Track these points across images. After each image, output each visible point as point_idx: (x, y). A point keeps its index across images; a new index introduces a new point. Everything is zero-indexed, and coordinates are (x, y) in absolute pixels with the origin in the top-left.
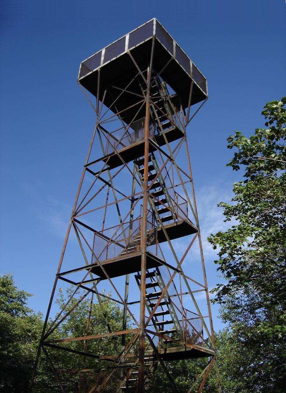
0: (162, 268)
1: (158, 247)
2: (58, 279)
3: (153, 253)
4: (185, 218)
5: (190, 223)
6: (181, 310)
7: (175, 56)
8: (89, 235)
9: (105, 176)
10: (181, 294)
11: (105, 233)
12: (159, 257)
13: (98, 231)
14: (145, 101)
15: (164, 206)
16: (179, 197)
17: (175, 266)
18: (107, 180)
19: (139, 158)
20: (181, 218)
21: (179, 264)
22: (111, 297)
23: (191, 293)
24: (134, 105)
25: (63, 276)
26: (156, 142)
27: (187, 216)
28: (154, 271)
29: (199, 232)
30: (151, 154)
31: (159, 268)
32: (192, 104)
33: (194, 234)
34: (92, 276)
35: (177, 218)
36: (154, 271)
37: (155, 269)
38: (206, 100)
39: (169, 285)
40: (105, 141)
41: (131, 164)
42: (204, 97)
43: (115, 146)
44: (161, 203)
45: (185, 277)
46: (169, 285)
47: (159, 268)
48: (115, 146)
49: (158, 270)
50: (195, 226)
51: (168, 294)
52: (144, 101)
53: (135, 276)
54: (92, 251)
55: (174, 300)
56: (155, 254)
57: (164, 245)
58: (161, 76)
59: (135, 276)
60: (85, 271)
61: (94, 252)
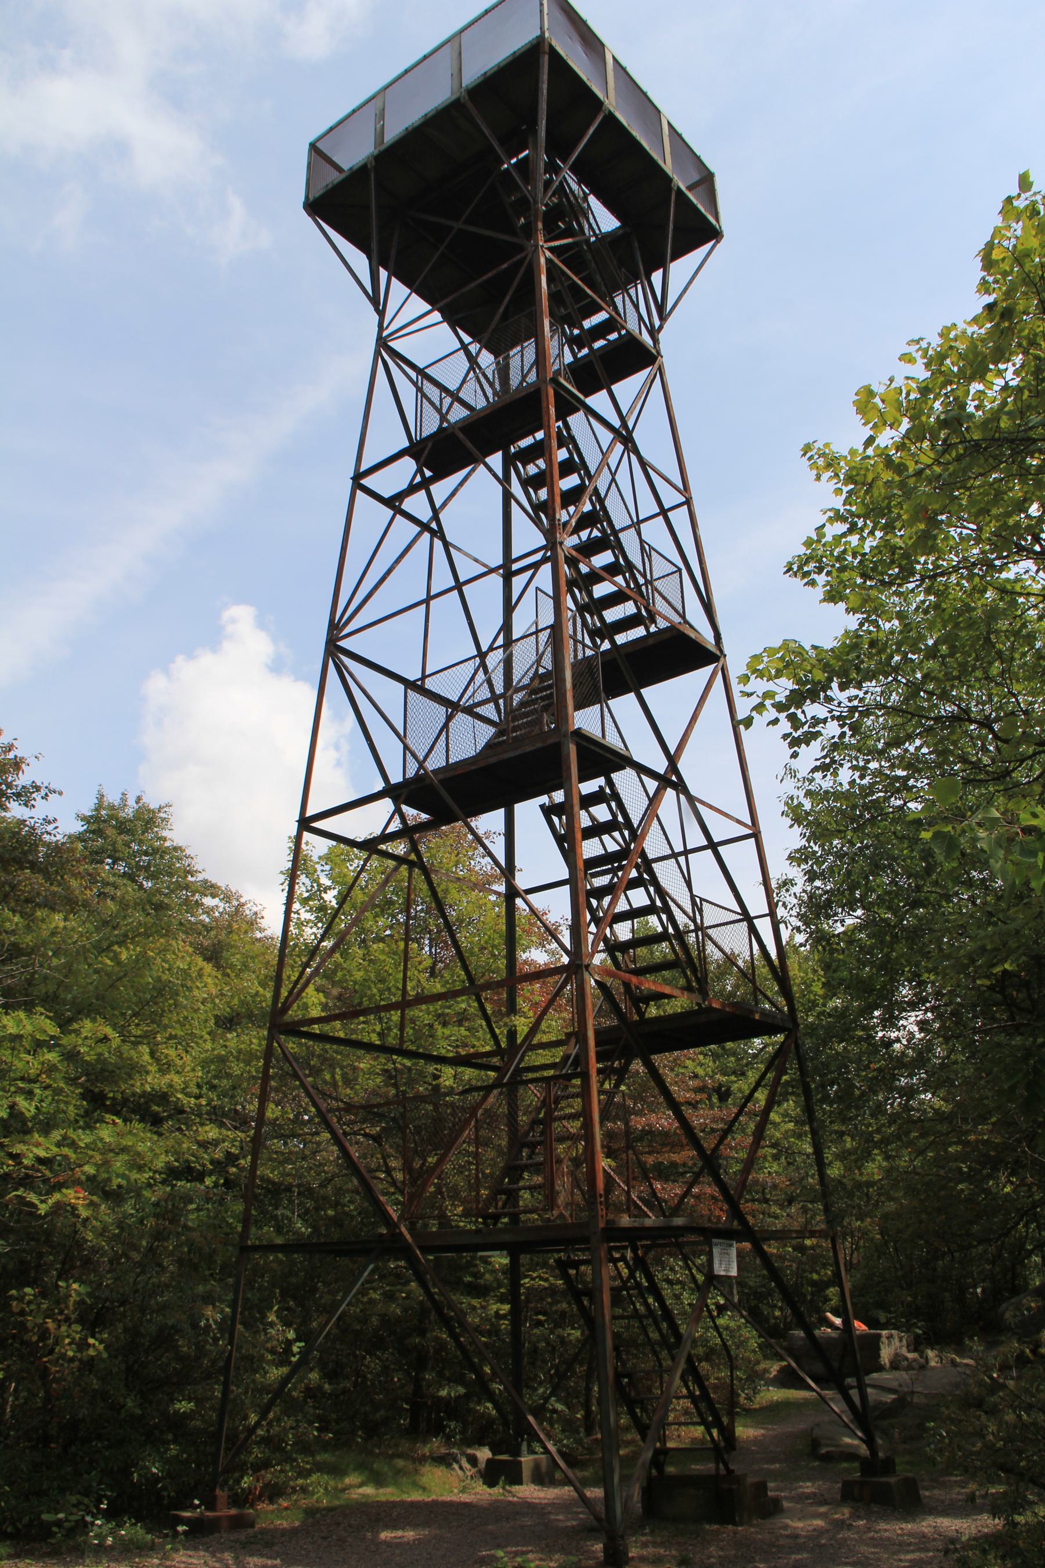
0: (625, 780)
1: (606, 710)
4: (677, 619)
5: (693, 635)
9: (417, 505)
10: (686, 852)
11: (430, 684)
12: (612, 740)
14: (529, 258)
17: (660, 765)
18: (425, 515)
19: (533, 441)
20: (666, 618)
21: (672, 760)
23: (713, 846)
24: (494, 272)
25: (317, 825)
26: (570, 383)
27: (683, 616)
28: (600, 787)
29: (722, 659)
30: (560, 423)
31: (615, 776)
32: (675, 257)
33: (709, 669)
34: (403, 818)
35: (654, 621)
36: (600, 787)
37: (601, 781)
39: (599, 470)
41: (496, 460)
44: (604, 574)
46: (599, 470)
47: (615, 776)
49: (610, 783)
50: (707, 635)
53: (542, 807)
54: (402, 739)
55: (667, 874)
57: (624, 705)
58: (574, 169)
59: (542, 807)
60: (386, 805)
61: (408, 741)
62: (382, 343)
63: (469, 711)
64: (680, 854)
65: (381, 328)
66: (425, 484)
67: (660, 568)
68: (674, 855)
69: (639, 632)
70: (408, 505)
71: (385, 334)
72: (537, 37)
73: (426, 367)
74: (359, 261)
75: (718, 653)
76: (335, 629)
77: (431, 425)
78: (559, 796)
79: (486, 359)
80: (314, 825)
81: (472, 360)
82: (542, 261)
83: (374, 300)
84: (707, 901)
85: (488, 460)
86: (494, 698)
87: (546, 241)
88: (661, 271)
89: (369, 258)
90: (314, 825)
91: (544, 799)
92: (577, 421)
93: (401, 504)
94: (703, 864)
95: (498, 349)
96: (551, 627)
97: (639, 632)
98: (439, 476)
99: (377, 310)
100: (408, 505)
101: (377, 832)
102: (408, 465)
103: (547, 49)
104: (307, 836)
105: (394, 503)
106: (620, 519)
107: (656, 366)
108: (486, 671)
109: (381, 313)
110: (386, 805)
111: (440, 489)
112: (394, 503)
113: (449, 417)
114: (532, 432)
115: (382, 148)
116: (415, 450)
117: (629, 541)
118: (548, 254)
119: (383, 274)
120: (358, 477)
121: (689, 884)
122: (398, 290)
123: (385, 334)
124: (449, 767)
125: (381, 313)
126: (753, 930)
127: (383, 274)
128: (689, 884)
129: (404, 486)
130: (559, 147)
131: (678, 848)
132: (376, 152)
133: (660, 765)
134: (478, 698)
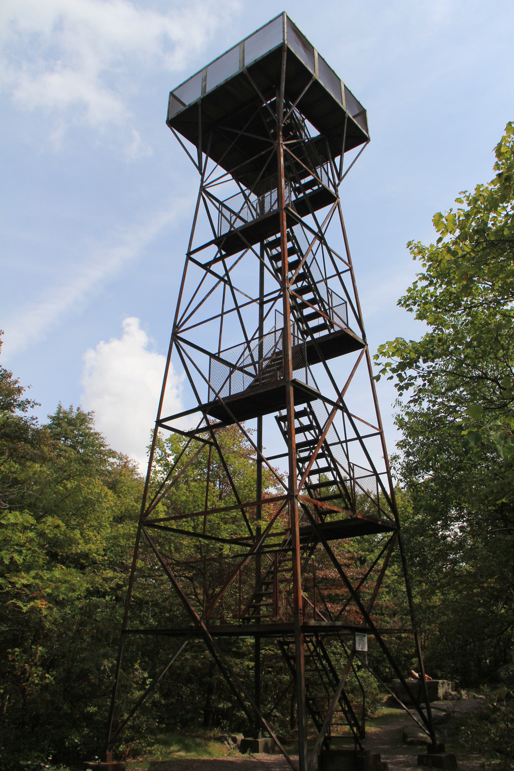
0: (317, 405)
1: (308, 370)
2: (324, 322)
3: (302, 380)
4: (344, 326)
5: (352, 334)
6: (347, 469)
7: (318, 75)
8: (202, 360)
9: (218, 268)
10: (346, 441)
11: (222, 356)
12: (311, 385)
13: (213, 352)
15: (314, 308)
16: (333, 294)
17: (334, 398)
18: (222, 273)
20: (338, 326)
21: (340, 396)
22: (248, 434)
23: (359, 438)
25: (165, 423)
26: (294, 210)
27: (347, 325)
28: (305, 408)
30: (289, 230)
32: (347, 150)
34: (207, 421)
35: (333, 327)
36: (305, 408)
37: (305, 405)
38: (367, 143)
39: (307, 253)
40: (214, 213)
41: (257, 247)
42: (365, 139)
43: (231, 219)
45: (350, 416)
46: (307, 253)
48: (231, 219)
49: (310, 406)
51: (325, 442)
52: (273, 149)
53: (276, 417)
54: (208, 382)
56: (305, 383)
57: (317, 368)
59: (276, 417)
61: (211, 384)
62: (203, 189)
63: (241, 369)
64: (343, 442)
65: (202, 181)
66: (222, 258)
67: (336, 301)
68: (340, 442)
69: (325, 332)
70: (213, 268)
71: (204, 184)
72: (281, 44)
73: (224, 201)
74: (193, 149)
75: (364, 344)
76: (176, 328)
77: (225, 229)
78: (284, 412)
79: (253, 198)
80: (164, 423)
81: (246, 198)
82: (282, 150)
83: (199, 168)
84: (356, 465)
85: (253, 247)
86: (254, 363)
87: (283, 141)
88: (339, 157)
89: (197, 147)
90: (164, 423)
91: (277, 413)
92: (297, 229)
93: (210, 267)
94: (354, 447)
95: (259, 193)
96: (282, 329)
97: (325, 332)
98: (229, 254)
99: (201, 173)
100: (213, 268)
101: (195, 428)
102: (214, 249)
103: (286, 49)
104: (160, 429)
105: (206, 267)
106: (317, 277)
107: (336, 202)
108: (250, 350)
109: (203, 175)
110: (199, 415)
111: (230, 261)
112: (206, 267)
113: (234, 226)
114: (275, 234)
115: (205, 95)
116: (218, 241)
117: (321, 287)
118: (284, 147)
119: (204, 155)
120: (189, 254)
121: (347, 456)
122: (211, 163)
123: (204, 184)
124: (230, 397)
125: (203, 175)
126: (378, 480)
127: (204, 155)
128: (347, 456)
129: (212, 258)
130: (291, 96)
131: (343, 439)
132: (202, 97)
133: (334, 398)
134: (246, 363)
